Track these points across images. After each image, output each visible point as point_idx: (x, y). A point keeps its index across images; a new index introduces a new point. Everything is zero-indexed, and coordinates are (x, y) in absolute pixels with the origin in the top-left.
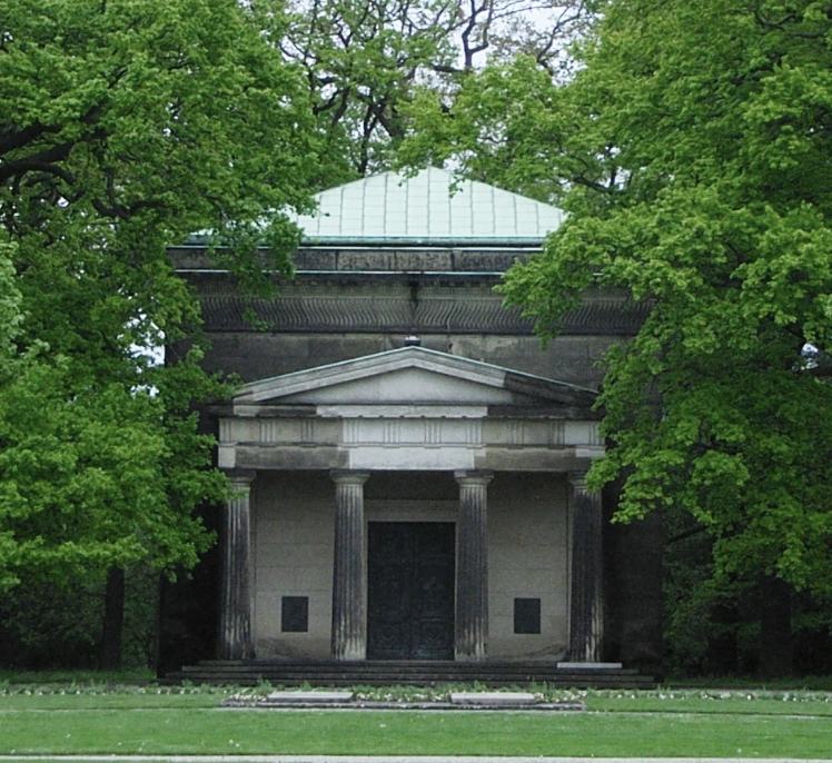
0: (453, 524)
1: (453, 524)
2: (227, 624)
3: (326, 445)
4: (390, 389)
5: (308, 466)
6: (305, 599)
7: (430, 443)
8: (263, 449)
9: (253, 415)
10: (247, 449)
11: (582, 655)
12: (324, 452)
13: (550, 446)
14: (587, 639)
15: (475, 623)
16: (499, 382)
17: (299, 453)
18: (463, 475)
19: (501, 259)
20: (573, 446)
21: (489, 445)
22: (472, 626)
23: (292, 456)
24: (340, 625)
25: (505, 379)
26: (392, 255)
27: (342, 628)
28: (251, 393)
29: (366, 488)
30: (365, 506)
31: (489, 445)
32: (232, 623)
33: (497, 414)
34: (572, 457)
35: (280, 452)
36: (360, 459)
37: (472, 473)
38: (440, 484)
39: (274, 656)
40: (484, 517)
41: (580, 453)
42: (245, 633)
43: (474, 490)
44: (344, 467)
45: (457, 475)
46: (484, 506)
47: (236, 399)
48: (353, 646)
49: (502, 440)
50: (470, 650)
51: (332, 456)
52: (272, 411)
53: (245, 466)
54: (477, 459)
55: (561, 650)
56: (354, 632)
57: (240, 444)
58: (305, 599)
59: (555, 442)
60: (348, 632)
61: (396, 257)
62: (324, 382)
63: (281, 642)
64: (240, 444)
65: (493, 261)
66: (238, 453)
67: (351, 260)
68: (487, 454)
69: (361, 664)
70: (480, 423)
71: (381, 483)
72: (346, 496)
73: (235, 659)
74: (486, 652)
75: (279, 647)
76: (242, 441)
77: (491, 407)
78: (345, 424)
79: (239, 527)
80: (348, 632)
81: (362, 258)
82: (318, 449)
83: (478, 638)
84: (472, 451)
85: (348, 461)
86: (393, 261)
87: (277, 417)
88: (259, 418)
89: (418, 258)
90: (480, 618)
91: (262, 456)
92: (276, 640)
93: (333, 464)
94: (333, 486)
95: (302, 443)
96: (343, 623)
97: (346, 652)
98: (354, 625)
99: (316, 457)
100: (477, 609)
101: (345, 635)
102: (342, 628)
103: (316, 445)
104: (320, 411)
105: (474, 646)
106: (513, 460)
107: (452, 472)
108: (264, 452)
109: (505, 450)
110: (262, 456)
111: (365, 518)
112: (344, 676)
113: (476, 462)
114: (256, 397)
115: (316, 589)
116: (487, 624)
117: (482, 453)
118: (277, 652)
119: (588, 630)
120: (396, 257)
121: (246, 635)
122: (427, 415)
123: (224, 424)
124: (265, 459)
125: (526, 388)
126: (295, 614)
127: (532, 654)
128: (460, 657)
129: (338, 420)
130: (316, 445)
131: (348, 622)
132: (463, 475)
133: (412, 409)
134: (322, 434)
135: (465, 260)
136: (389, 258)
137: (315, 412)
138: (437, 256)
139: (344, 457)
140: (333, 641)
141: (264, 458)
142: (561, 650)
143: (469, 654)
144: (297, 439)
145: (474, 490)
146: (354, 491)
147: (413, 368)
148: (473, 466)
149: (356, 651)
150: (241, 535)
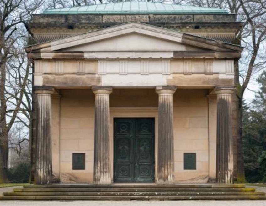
0: (153, 119)
1: (153, 119)
2: (39, 166)
3: (89, 74)
4: (122, 44)
5: (80, 85)
6: (84, 154)
7: (143, 72)
8: (57, 76)
9: (51, 58)
10: (49, 76)
11: (223, 181)
12: (88, 78)
13: (205, 73)
14: (226, 172)
15: (168, 165)
16: (179, 40)
17: (76, 78)
18: (161, 88)
19: (169, 18)
20: (217, 73)
21: (174, 73)
22: (166, 166)
23: (72, 79)
24: (98, 166)
25: (182, 38)
26: (125, 16)
27: (99, 168)
28: (50, 46)
29: (111, 96)
30: (111, 110)
31: (174, 73)
32: (42, 166)
33: (178, 57)
34: (217, 79)
35: (66, 78)
36: (106, 81)
37: (166, 87)
38: (148, 95)
39: (69, 181)
40: (172, 110)
41: (221, 77)
42: (49, 171)
43: (167, 97)
44: (100, 85)
45: (158, 88)
46: (172, 105)
47: (42, 50)
48: (105, 177)
49: (181, 71)
50: (165, 179)
51: (93, 79)
52: (61, 56)
53: (47, 85)
54: (168, 80)
55: (206, 177)
56: (105, 170)
57: (45, 74)
58: (84, 154)
59: (208, 71)
60: (102, 170)
61: (126, 17)
62: (88, 40)
63: (73, 175)
64: (45, 74)
65: (166, 19)
66: (44, 78)
67: (108, 19)
68: (173, 77)
69: (109, 187)
70: (169, 61)
71: (120, 95)
72: (100, 101)
73: (43, 184)
74: (173, 180)
75: (72, 178)
76: (47, 72)
77: (175, 52)
78: (99, 61)
79: (45, 116)
80: (102, 170)
81: (112, 18)
82: (86, 76)
83: (169, 173)
84: (165, 76)
85: (101, 82)
86: (125, 19)
87: (64, 59)
88: (54, 60)
89: (135, 18)
90: (170, 162)
91: (56, 80)
92: (70, 174)
93: (93, 84)
94: (93, 96)
95: (78, 73)
96: (99, 165)
97: (101, 180)
98: (105, 166)
99: (85, 81)
100: (167, 158)
101: (101, 172)
102: (99, 168)
103: (85, 74)
104: (86, 55)
105: (167, 177)
106: (187, 81)
107: (155, 87)
108: (57, 78)
109: (182, 75)
110: (56, 80)
111: (111, 116)
112: (99, 193)
113: (167, 82)
114: (53, 48)
115: (87, 148)
116: (173, 165)
117: (171, 77)
118: (70, 180)
119: (226, 168)
120: (126, 17)
121: (50, 172)
122: (142, 57)
123: (37, 63)
124: (58, 82)
125: (193, 43)
126: (79, 161)
127: (192, 179)
128: (159, 182)
129: (95, 60)
130: (85, 74)
131: (102, 165)
132: (161, 88)
133: (134, 53)
134: (88, 68)
135: (155, 18)
136: (124, 18)
137: (83, 56)
138: (143, 17)
139: (99, 80)
140: (95, 173)
141: (58, 81)
142: (206, 177)
143: (165, 181)
144: (75, 71)
145: (167, 97)
146: (104, 98)
147: (134, 33)
148: (165, 84)
149: (106, 179)
150: (47, 121)
